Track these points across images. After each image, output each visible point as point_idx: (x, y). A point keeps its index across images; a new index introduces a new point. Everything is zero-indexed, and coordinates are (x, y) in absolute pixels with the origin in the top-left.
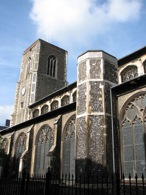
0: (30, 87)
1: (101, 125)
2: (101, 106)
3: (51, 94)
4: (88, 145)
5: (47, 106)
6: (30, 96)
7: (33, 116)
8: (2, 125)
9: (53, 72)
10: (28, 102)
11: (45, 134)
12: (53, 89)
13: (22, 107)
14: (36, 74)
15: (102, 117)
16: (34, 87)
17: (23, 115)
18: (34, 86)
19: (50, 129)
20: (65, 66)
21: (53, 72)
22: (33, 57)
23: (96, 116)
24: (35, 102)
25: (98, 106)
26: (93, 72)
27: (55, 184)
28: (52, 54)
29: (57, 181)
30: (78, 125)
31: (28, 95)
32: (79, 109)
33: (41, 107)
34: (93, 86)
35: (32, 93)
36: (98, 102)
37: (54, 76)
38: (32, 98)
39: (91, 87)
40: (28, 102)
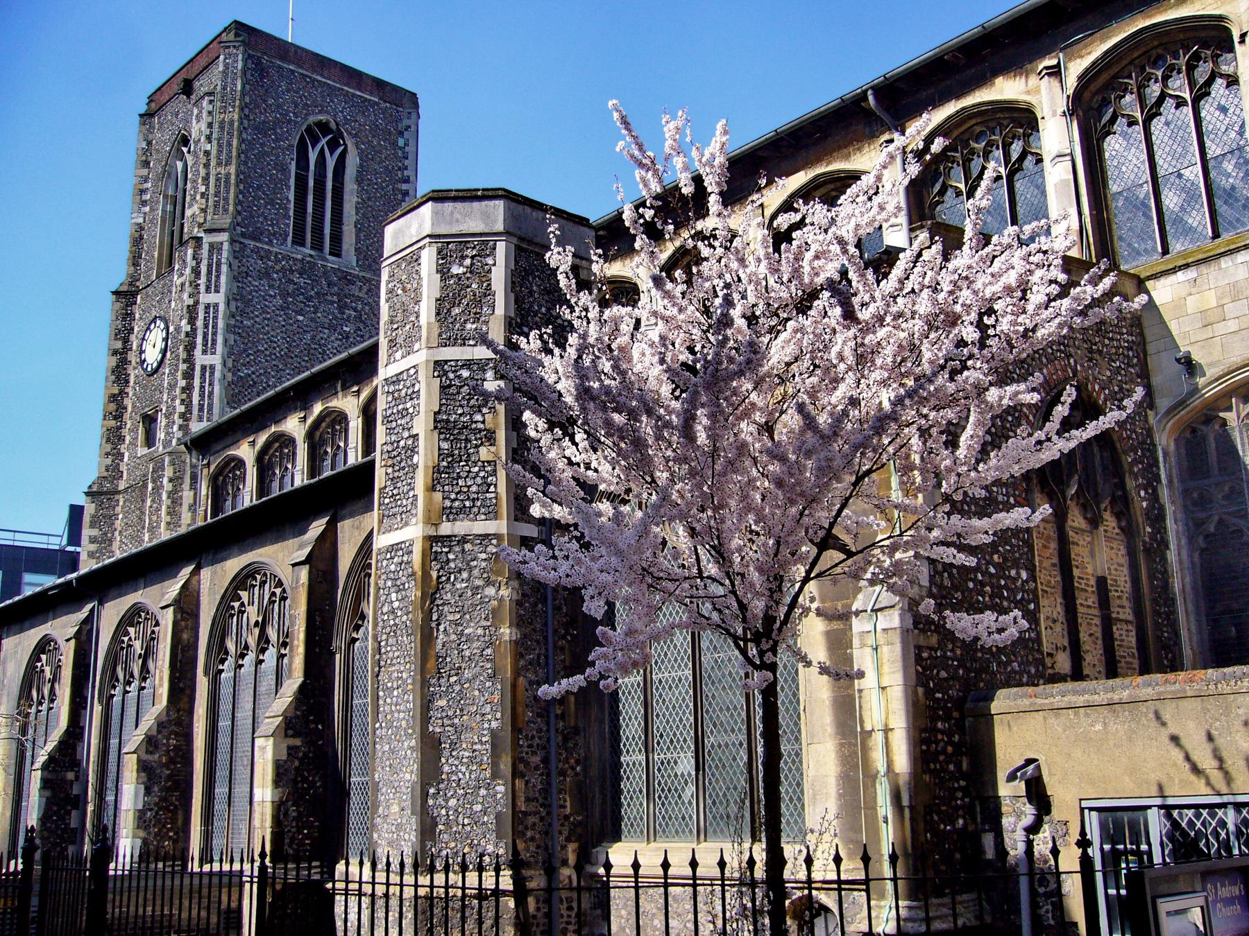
0: (192, 321)
1: (489, 582)
2: (492, 489)
3: (307, 374)
4: (425, 683)
5: (286, 441)
6: (188, 375)
7: (217, 507)
8: (44, 539)
9: (327, 230)
10: (182, 416)
11: (253, 614)
12: (332, 328)
13: (150, 441)
14: (226, 246)
15: (494, 542)
16: (215, 326)
17: (157, 489)
18: (215, 318)
19: (278, 591)
20: (404, 187)
21: (327, 230)
22: (203, 139)
23: (464, 540)
24: (222, 413)
25: (474, 489)
26: (456, 311)
27: (206, 874)
28: (322, 117)
29: (314, 864)
30: (381, 583)
31: (179, 374)
32: (387, 501)
33: (253, 443)
34: (450, 386)
35: (200, 359)
36: (476, 469)
37: (336, 251)
38: (202, 387)
39: (443, 388)
40: (182, 416)
